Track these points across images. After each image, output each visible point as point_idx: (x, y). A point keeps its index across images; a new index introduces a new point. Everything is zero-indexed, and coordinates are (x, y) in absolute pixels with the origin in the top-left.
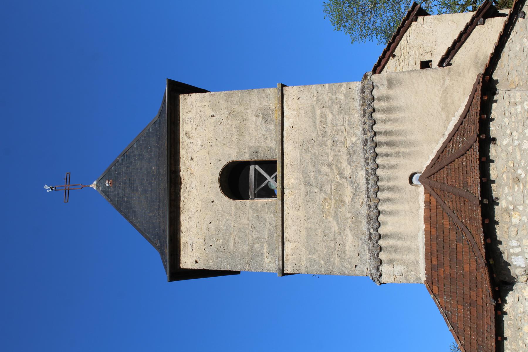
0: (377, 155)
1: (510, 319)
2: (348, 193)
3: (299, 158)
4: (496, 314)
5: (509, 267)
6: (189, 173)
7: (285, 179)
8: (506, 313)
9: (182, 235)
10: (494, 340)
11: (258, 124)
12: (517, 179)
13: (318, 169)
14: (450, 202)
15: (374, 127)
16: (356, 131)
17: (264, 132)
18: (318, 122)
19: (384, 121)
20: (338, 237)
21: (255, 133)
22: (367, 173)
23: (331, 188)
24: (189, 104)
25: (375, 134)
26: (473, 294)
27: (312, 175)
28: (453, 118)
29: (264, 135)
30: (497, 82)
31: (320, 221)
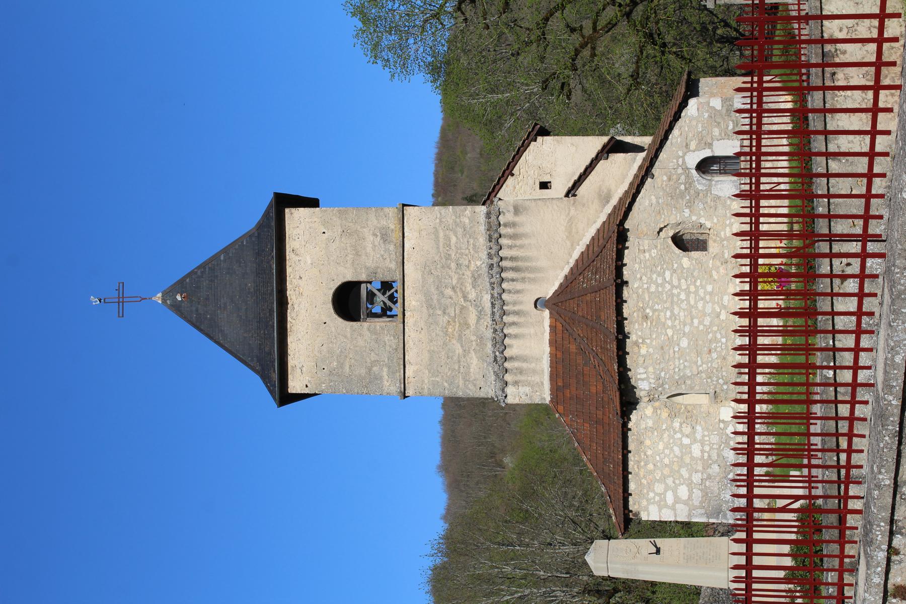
0: (503, 280)
1: (634, 435)
2: (472, 318)
3: (421, 281)
4: (623, 430)
5: (635, 390)
6: (297, 293)
7: (406, 301)
8: (630, 430)
9: (289, 358)
10: (621, 454)
11: (376, 243)
12: (646, 317)
13: (441, 292)
14: (580, 330)
15: (500, 253)
16: (481, 255)
17: (382, 253)
18: (441, 245)
19: (510, 247)
20: (463, 359)
21: (372, 253)
22: (492, 296)
23: (455, 311)
24: (297, 219)
25: (501, 259)
26: (600, 413)
27: (435, 297)
28: (577, 247)
29: (382, 256)
30: (628, 230)
31: (444, 344)
